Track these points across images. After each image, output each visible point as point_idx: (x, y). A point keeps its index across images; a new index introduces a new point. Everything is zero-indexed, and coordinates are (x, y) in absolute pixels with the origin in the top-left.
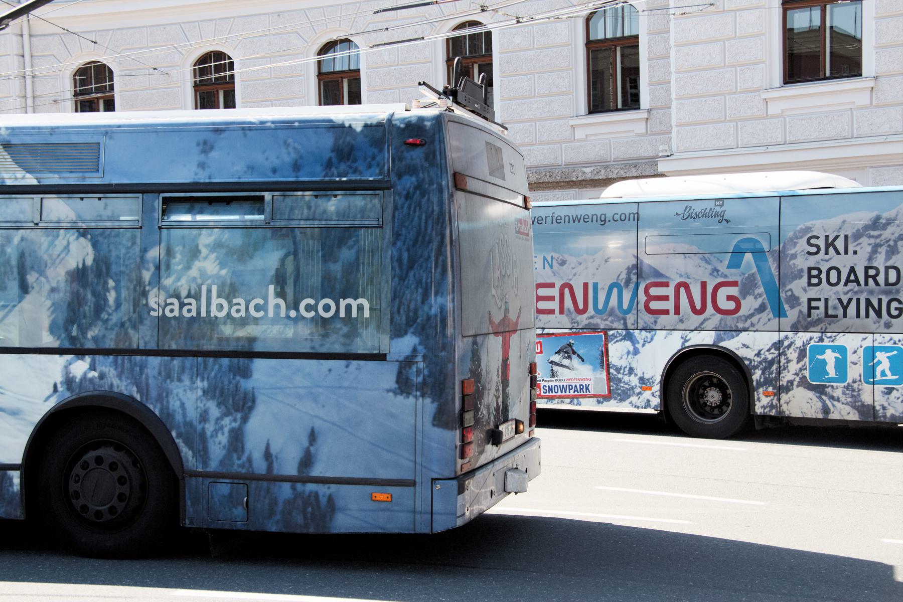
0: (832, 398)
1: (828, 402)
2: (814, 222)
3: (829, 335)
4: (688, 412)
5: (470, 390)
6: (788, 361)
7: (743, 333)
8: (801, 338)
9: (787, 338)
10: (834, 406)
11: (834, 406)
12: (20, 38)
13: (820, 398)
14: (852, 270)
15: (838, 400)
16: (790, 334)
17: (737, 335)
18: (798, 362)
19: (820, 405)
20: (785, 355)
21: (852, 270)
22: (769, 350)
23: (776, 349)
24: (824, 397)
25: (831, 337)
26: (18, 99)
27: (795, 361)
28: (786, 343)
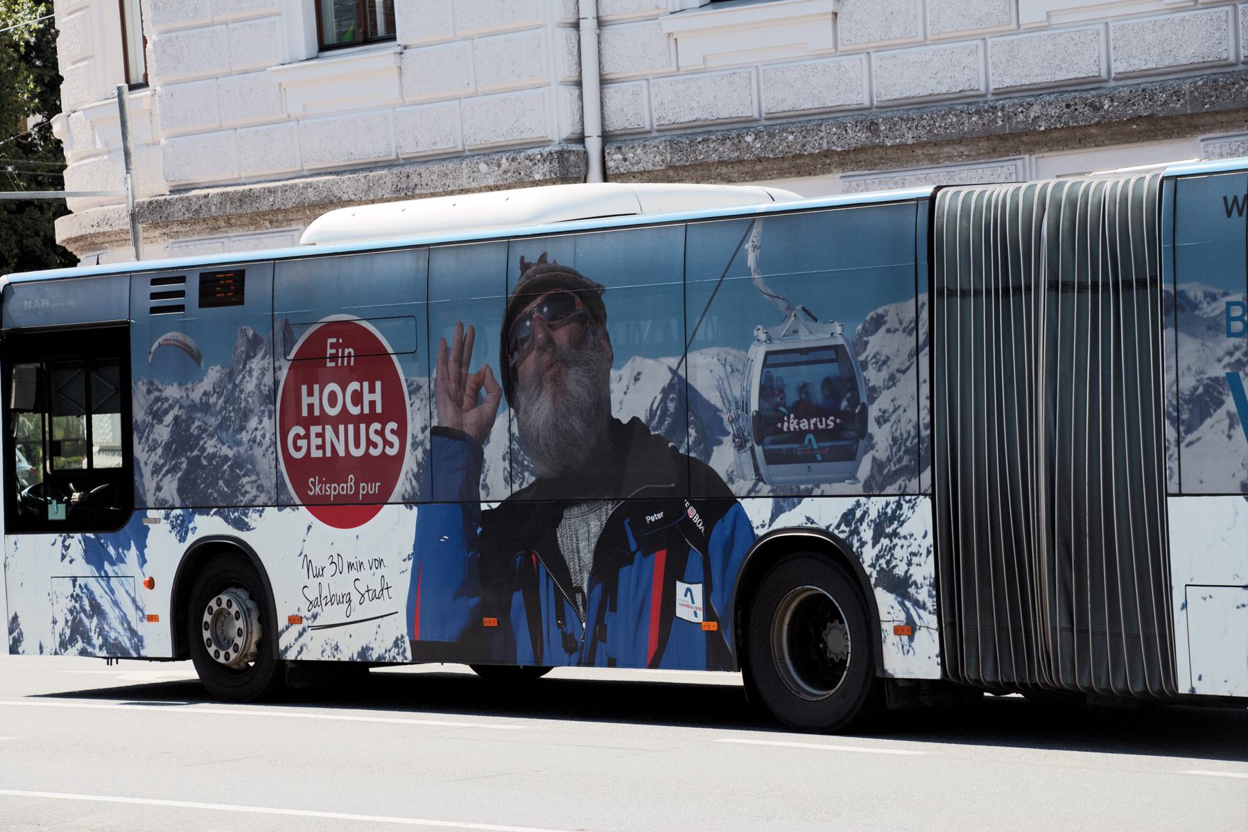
0: (917, 603)
1: (912, 611)
2: (886, 307)
3: (907, 498)
4: (782, 604)
5: (1053, 293)
6: (863, 544)
7: (806, 500)
8: (875, 506)
9: (858, 505)
10: (920, 617)
11: (920, 617)
12: (572, 32)
13: (902, 604)
14: (1235, 197)
15: (924, 607)
16: (863, 500)
17: (799, 503)
18: (874, 546)
19: (902, 616)
20: (858, 534)
21: (1235, 197)
22: (838, 527)
23: (847, 525)
24: (908, 604)
25: (910, 501)
26: (562, 88)
27: (870, 542)
28: (858, 514)
